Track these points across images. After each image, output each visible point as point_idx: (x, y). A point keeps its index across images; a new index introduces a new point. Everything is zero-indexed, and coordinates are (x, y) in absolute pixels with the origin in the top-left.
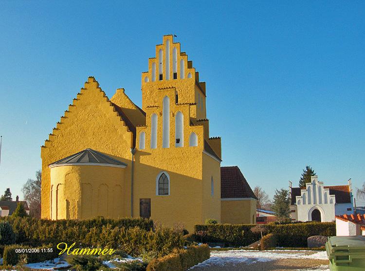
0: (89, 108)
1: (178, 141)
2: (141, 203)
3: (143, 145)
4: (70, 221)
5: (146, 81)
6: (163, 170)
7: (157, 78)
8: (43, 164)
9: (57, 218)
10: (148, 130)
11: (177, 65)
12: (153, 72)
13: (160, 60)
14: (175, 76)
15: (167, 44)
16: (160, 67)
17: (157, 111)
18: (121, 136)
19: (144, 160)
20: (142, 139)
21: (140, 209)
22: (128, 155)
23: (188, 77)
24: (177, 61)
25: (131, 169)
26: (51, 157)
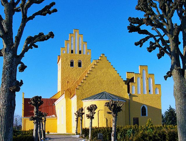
0: (103, 70)
1: (149, 91)
2: (134, 120)
3: (133, 91)
4: (92, 129)
5: (63, 52)
6: (144, 104)
7: (69, 52)
8: (77, 98)
9: (91, 126)
10: (136, 85)
11: (81, 47)
12: (67, 48)
13: (72, 42)
14: (80, 52)
15: (76, 34)
16: (71, 46)
17: (140, 76)
18: (122, 87)
19: (134, 99)
20: (132, 89)
21: (67, 121)
22: (127, 96)
23: (88, 54)
24: (81, 44)
25: (128, 103)
26: (83, 94)
